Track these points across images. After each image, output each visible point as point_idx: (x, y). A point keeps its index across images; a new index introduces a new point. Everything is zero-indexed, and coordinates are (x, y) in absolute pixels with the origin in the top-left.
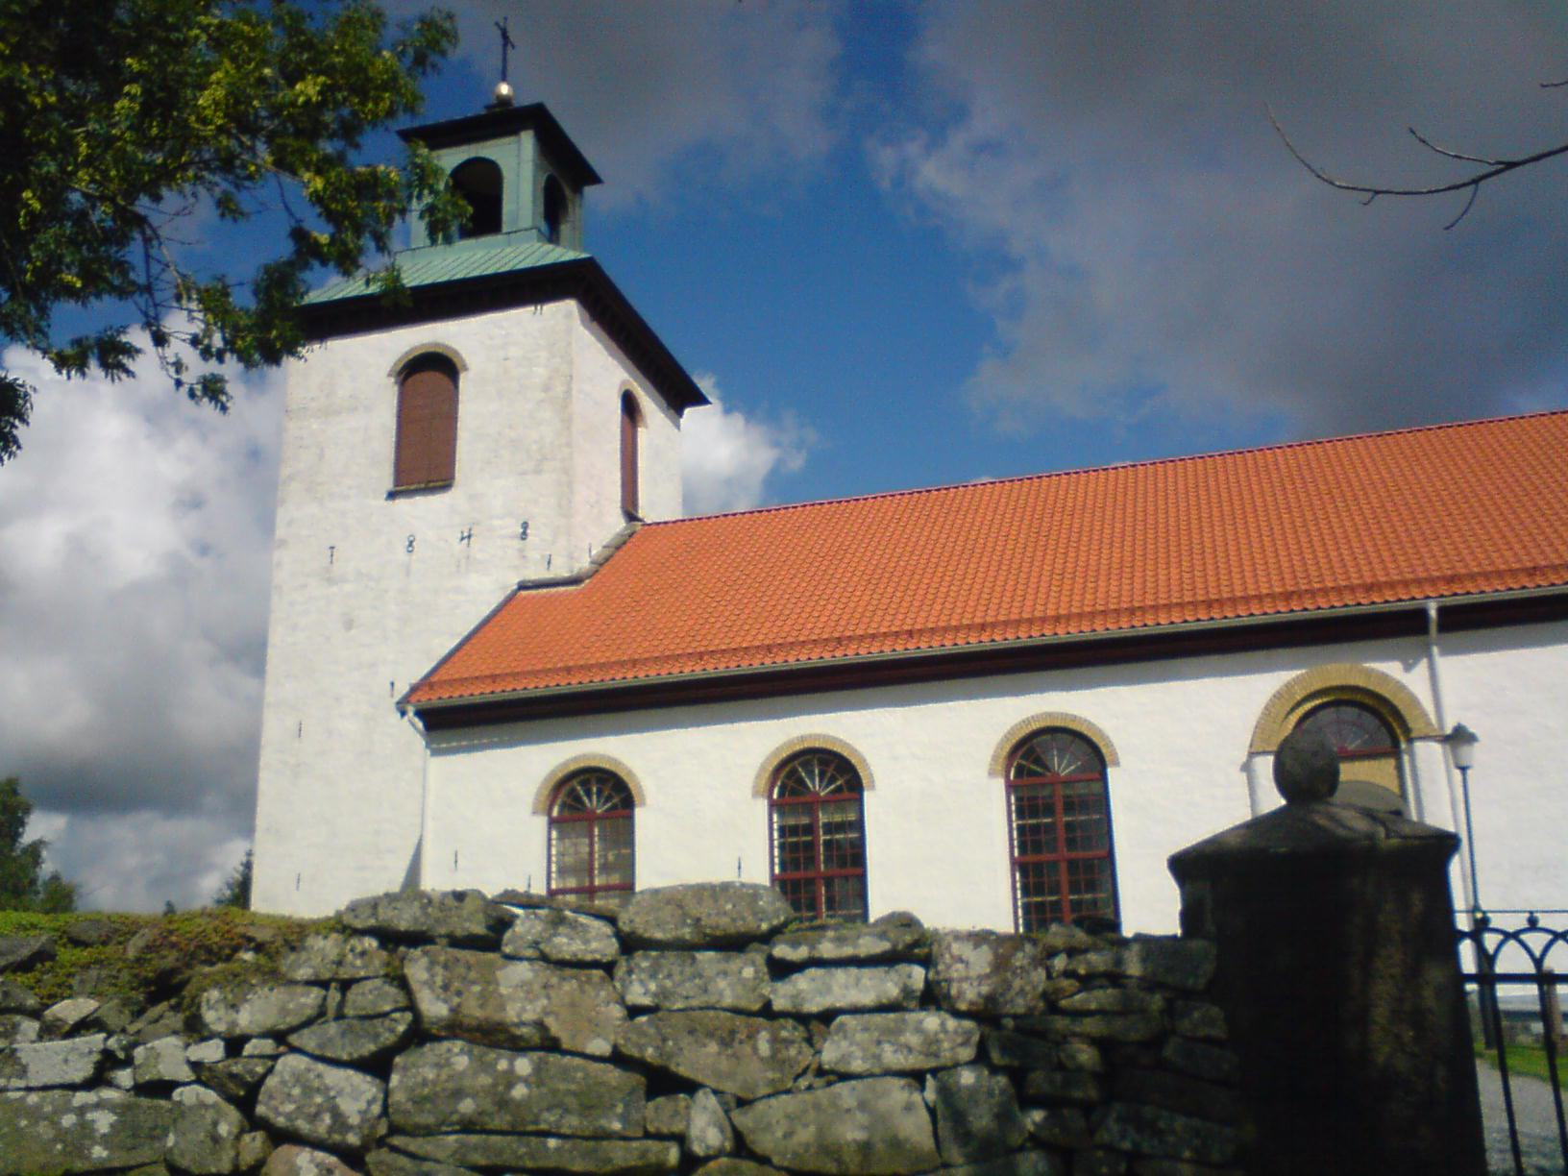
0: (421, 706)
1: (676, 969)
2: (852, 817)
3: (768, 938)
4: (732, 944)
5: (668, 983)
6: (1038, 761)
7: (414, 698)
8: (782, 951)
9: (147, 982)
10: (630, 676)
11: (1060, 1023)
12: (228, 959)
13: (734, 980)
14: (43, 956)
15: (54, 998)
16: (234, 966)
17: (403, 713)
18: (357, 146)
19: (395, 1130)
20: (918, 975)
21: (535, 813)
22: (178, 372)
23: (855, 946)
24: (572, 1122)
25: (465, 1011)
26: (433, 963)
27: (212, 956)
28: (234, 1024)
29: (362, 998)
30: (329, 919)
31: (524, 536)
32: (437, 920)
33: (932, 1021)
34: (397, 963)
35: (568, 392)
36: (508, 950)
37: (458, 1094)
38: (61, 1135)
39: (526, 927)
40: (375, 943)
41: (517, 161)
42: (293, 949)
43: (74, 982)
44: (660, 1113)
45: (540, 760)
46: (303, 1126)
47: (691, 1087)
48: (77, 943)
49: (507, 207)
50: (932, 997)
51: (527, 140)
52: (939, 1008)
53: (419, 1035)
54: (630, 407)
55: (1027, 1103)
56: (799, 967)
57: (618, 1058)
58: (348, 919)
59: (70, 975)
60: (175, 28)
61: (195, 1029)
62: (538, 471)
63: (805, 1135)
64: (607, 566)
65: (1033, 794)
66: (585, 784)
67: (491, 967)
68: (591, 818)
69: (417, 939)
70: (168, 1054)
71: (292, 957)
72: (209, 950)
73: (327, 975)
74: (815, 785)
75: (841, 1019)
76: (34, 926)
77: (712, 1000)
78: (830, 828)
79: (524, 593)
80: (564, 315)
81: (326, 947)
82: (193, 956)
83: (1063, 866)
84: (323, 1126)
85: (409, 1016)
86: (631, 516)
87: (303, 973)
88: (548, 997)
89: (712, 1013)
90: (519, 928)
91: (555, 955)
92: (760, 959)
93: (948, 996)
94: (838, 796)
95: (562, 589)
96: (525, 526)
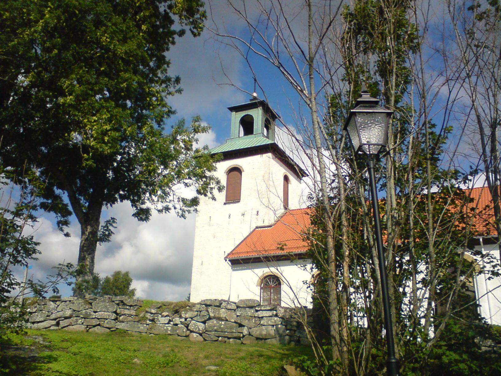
0: (231, 258)
3: (255, 307)
4: (251, 307)
8: (257, 308)
11: (292, 319)
13: (251, 312)
14: (160, 307)
17: (226, 260)
19: (206, 331)
20: (275, 312)
24: (229, 330)
27: (183, 307)
29: (202, 313)
30: (82, 226)
33: (276, 318)
37: (215, 326)
38: (165, 330)
39: (224, 304)
41: (258, 115)
44: (240, 329)
46: (194, 330)
47: (244, 326)
50: (276, 315)
53: (210, 319)
54: (286, 178)
55: (287, 330)
56: (259, 311)
57: (235, 322)
61: (181, 317)
63: (258, 333)
66: (269, 279)
68: (271, 287)
69: (210, 305)
70: (177, 320)
80: (267, 157)
81: (198, 306)
84: (197, 330)
86: (286, 206)
87: (195, 310)
96: (258, 212)
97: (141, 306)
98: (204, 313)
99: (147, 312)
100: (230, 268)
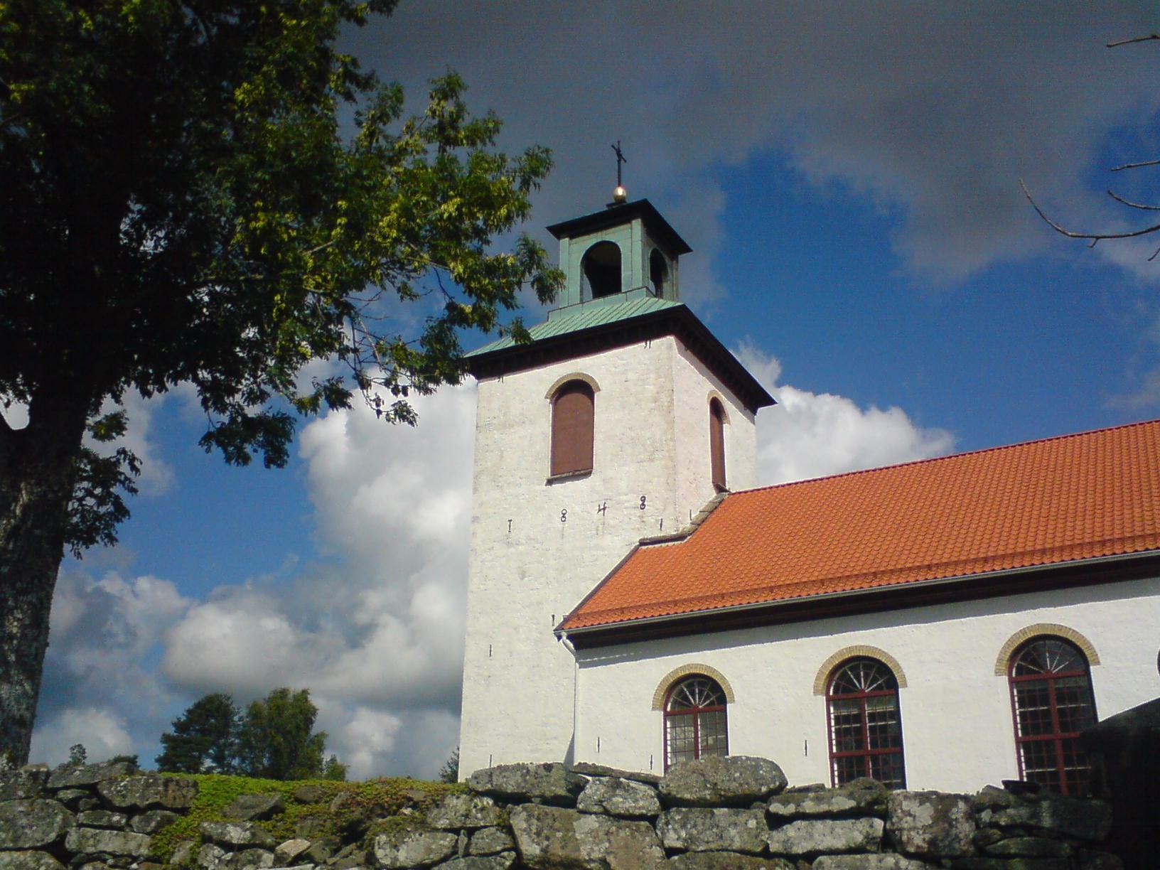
0: (574, 630)
1: (699, 821)
2: (891, 708)
4: (741, 802)
5: (695, 832)
6: (1034, 662)
7: (566, 627)
8: (776, 807)
9: (342, 829)
10: (720, 606)
12: (395, 813)
14: (277, 809)
15: (284, 838)
16: (397, 818)
17: (559, 638)
18: (488, 242)
20: (879, 824)
21: (654, 709)
22: (378, 405)
23: (830, 804)
25: (551, 850)
26: (530, 816)
27: (385, 811)
28: (396, 859)
29: (482, 841)
31: (643, 506)
32: (533, 785)
34: (505, 816)
35: (671, 402)
36: (581, 806)
39: (594, 789)
40: (491, 802)
42: (437, 806)
43: (297, 828)
45: (655, 670)
48: (300, 801)
49: (625, 274)
50: (889, 842)
51: (637, 225)
52: (895, 851)
54: (717, 409)
56: (790, 819)
58: (473, 784)
59: (294, 823)
60: (368, 177)
62: (651, 460)
64: (704, 525)
65: (1031, 688)
66: (690, 687)
67: (570, 819)
68: (695, 712)
71: (435, 811)
72: (382, 807)
73: (459, 825)
74: (863, 686)
75: (821, 858)
76: (274, 789)
77: (726, 844)
78: (873, 717)
79: (644, 548)
80: (667, 346)
81: (457, 804)
82: (372, 811)
83: (1058, 744)
85: (513, 854)
86: (720, 488)
87: (443, 823)
88: (609, 841)
89: (725, 854)
90: (588, 791)
91: (614, 811)
92: (761, 814)
93: (900, 842)
94: (881, 693)
95: (670, 544)
96: (643, 499)
97: (184, 811)
98: (489, 839)
99: (207, 839)
100: (573, 658)
